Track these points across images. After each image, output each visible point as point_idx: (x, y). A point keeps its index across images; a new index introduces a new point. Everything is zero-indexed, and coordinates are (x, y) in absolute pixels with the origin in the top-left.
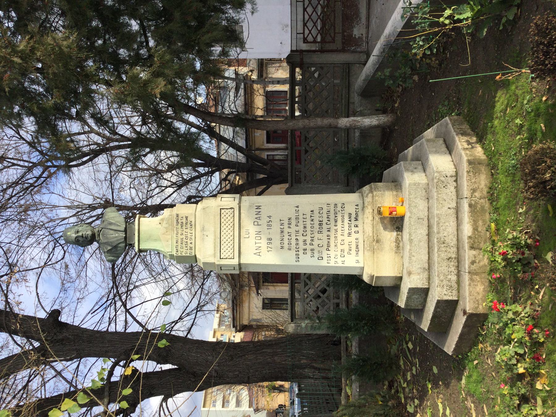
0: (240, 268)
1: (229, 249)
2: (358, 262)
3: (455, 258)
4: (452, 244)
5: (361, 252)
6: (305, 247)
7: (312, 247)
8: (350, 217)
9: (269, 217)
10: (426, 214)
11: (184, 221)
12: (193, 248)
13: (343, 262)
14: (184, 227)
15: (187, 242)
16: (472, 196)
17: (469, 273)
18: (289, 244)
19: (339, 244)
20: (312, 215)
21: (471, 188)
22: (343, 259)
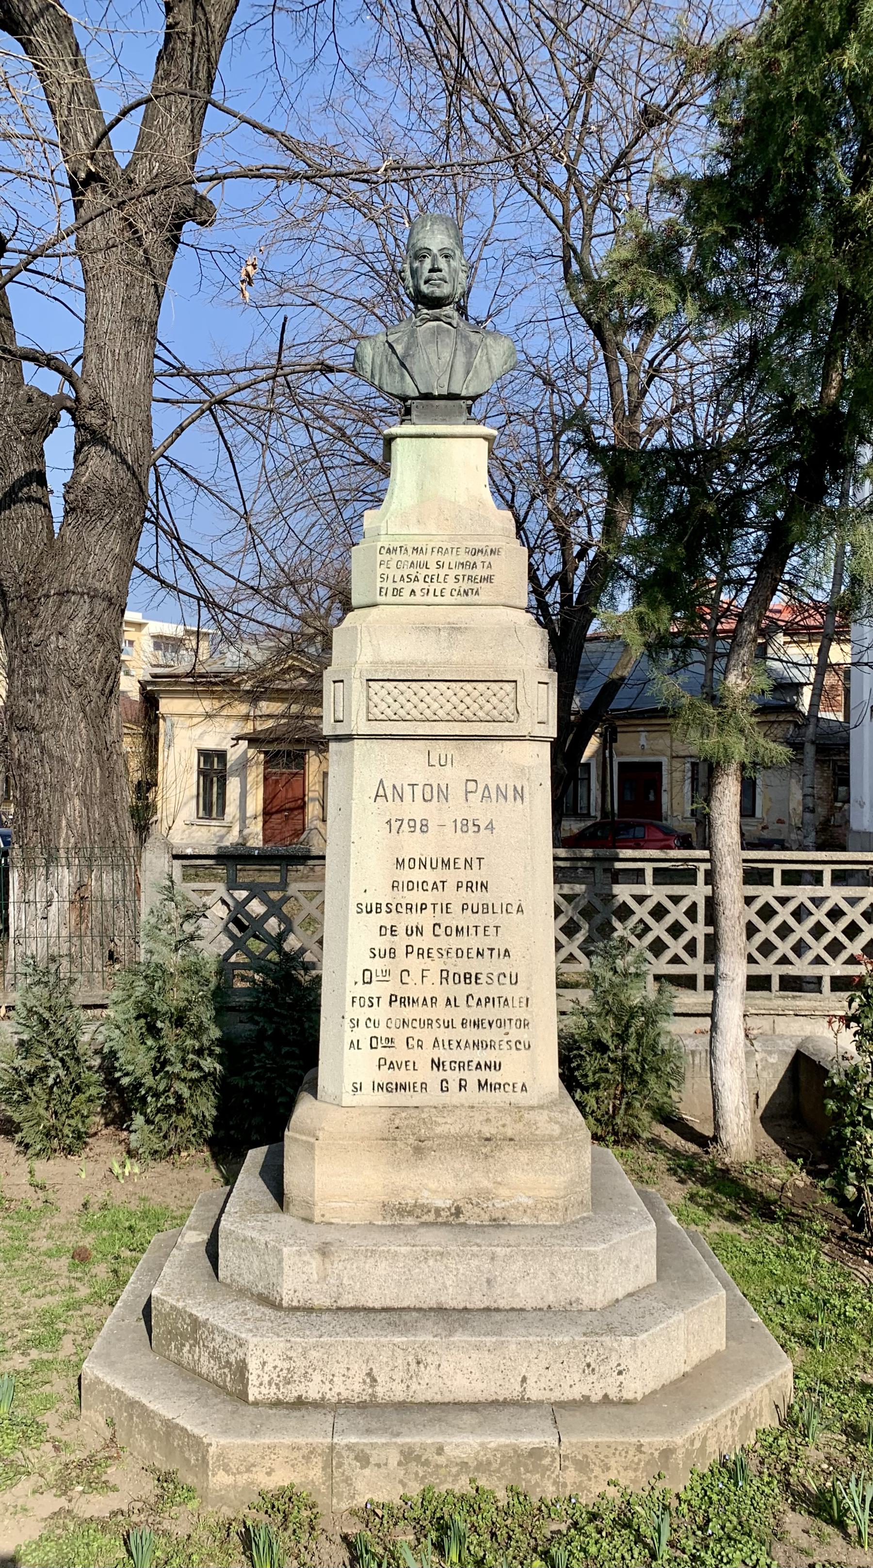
0: (339, 738)
1: (396, 706)
2: (357, 1088)
3: (373, 1395)
4: (414, 1386)
5: (382, 1098)
6: (401, 931)
7: (401, 952)
8: (488, 1066)
9: (490, 827)
10: (502, 1304)
11: (480, 572)
12: (397, 599)
13: (355, 1045)
14: (460, 571)
15: (416, 579)
16: (566, 1457)
17: (332, 1448)
18: (411, 886)
19: (408, 1031)
20: (495, 953)
21: (592, 1456)
22: (365, 1044)
